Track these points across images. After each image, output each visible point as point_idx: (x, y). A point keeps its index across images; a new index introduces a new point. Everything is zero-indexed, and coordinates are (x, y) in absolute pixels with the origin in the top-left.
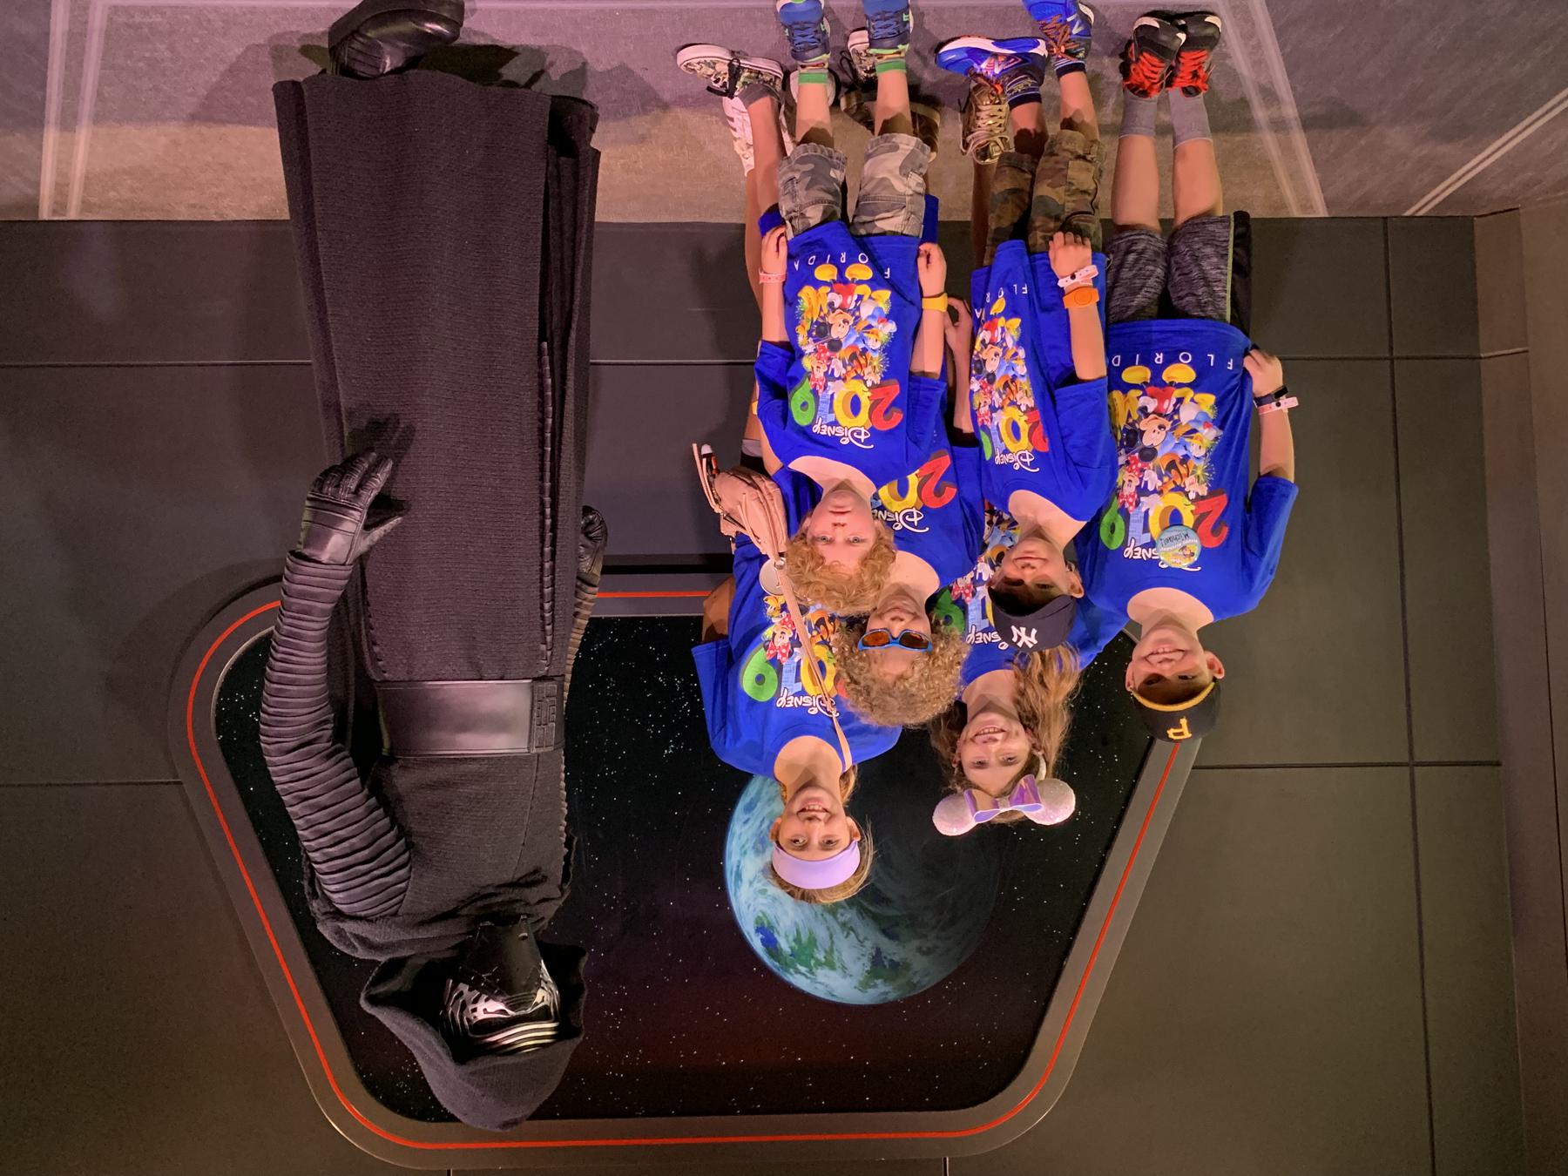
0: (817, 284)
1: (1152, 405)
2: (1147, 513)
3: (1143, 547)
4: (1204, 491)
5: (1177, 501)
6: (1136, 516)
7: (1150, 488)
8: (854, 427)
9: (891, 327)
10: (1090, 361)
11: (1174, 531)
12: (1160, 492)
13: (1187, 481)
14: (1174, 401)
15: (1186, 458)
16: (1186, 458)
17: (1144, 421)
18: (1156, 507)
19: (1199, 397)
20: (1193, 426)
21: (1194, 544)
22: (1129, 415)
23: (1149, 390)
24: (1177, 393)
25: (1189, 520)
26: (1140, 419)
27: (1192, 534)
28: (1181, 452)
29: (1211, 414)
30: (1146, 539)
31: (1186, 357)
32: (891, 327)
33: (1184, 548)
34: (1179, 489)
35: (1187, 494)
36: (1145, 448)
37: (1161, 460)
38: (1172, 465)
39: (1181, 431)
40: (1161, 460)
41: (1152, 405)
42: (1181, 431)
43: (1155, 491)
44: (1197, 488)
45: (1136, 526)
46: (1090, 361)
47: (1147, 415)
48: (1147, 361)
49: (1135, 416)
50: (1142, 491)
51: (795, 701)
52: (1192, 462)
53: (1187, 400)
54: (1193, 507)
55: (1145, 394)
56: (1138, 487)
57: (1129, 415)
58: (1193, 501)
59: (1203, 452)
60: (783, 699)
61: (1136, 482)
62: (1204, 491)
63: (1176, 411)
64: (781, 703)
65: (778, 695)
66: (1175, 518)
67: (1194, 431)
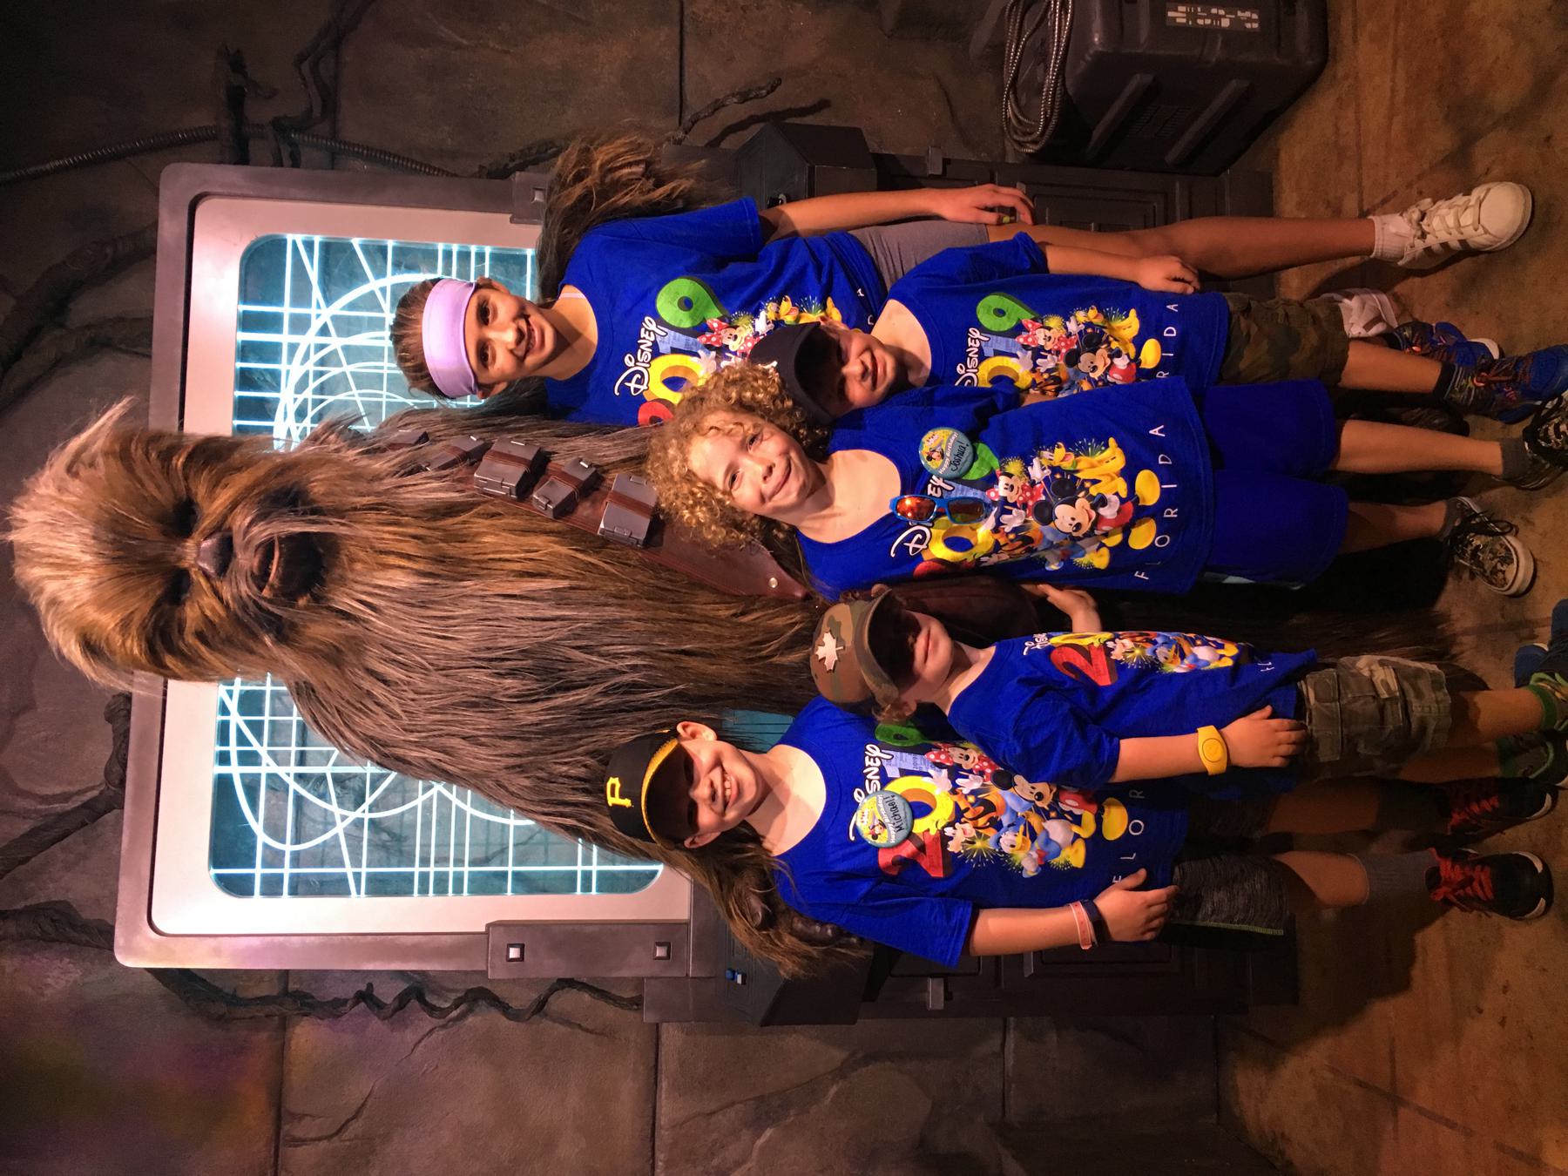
0: (1129, 474)
1: (1108, 512)
2: (1015, 356)
3: (980, 348)
4: (953, 847)
5: (944, 809)
6: (920, 762)
7: (1039, 361)
8: (871, 817)
9: (1030, 869)
10: (1138, 754)
11: (904, 812)
12: (1033, 370)
13: (968, 827)
14: (1077, 812)
15: (998, 826)
16: (998, 826)
17: (1087, 504)
18: (936, 786)
19: (1080, 848)
20: (1041, 837)
21: (888, 837)
22: (1095, 482)
23: (1129, 505)
24: (1088, 817)
25: (921, 826)
26: (1090, 498)
27: (904, 833)
28: (1005, 820)
29: (1058, 861)
30: (892, 772)
31: (1136, 828)
32: (1030, 869)
33: (883, 826)
34: (958, 815)
35: (951, 824)
36: (1052, 509)
37: (995, 795)
38: (989, 807)
39: (1035, 820)
40: (995, 795)
41: (1108, 512)
42: (1035, 820)
43: (1036, 365)
44: (959, 838)
45: (908, 761)
46: (1138, 754)
47: (1094, 507)
48: (1166, 498)
49: (1094, 491)
50: (955, 772)
51: (646, 341)
52: (991, 833)
53: (1075, 829)
54: (933, 832)
55: (1123, 501)
56: (959, 767)
57: (1095, 482)
58: (942, 832)
59: (1007, 849)
60: (653, 327)
61: (966, 765)
62: (953, 847)
63: (1061, 815)
64: (650, 324)
65: (660, 321)
66: (921, 809)
67: (1033, 837)
